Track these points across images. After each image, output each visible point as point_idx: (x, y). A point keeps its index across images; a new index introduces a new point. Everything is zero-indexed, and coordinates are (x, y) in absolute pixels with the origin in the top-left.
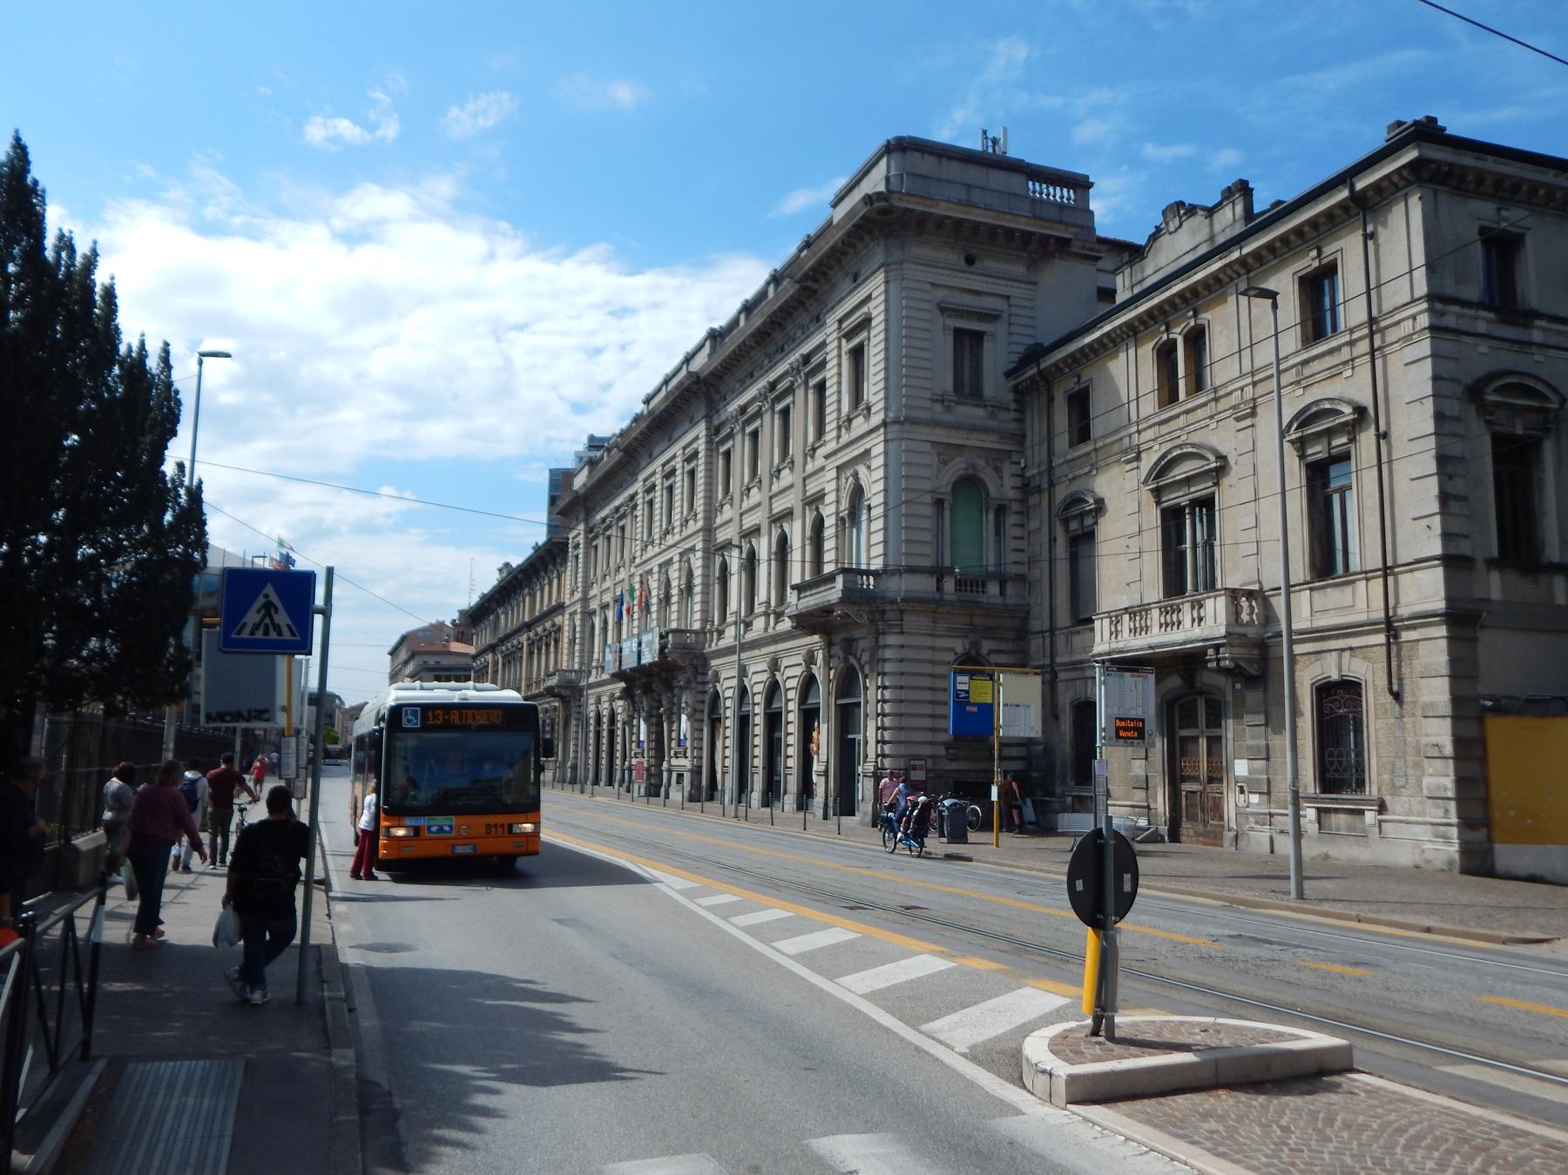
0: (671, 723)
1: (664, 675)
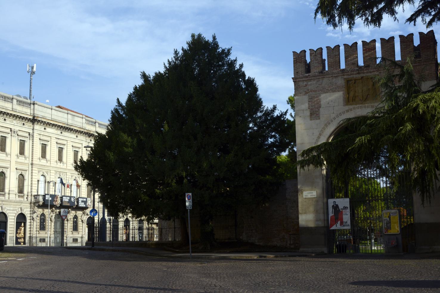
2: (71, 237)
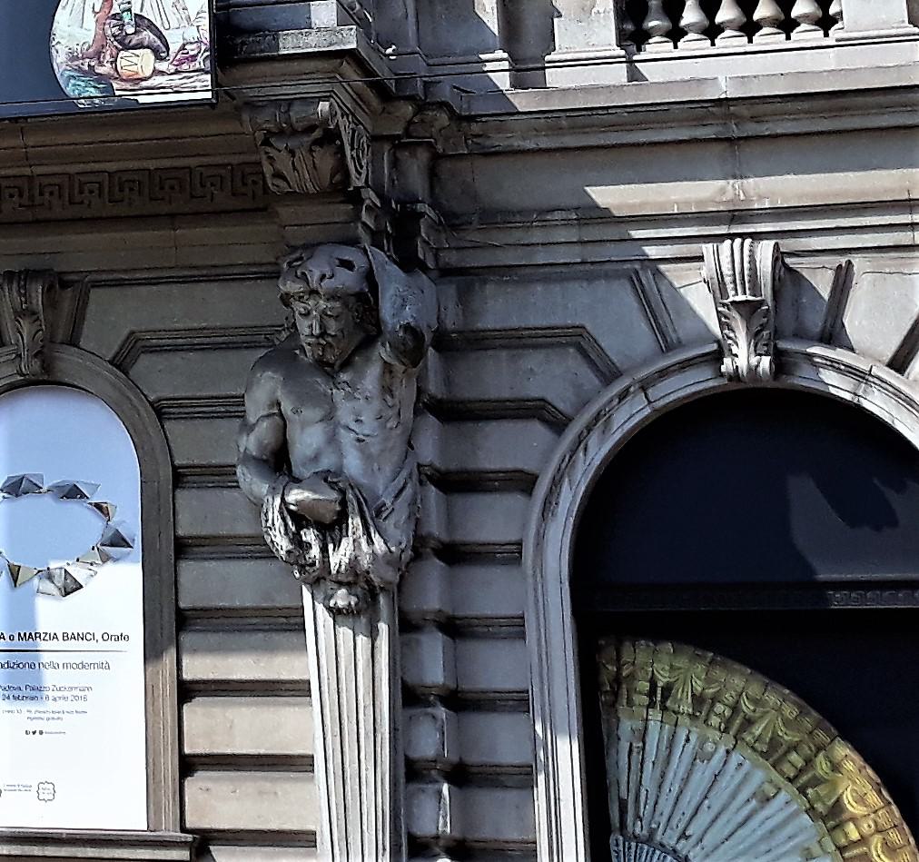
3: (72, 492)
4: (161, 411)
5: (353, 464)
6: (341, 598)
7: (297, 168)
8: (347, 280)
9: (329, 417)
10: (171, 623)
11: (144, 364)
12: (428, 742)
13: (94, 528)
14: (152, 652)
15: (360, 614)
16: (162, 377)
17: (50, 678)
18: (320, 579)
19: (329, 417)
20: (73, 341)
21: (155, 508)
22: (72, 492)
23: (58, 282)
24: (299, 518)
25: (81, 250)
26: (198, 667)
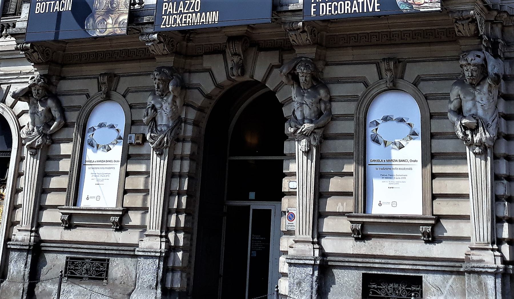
0: (46, 153)
1: (311, 52)
2: (62, 245)
3: (112, 127)
4: (131, 107)
5: (480, 112)
6: (477, 150)
7: (465, 29)
8: (478, 61)
9: (474, 99)
10: (429, 157)
11: (422, 84)
12: (501, 190)
13: (115, 135)
14: (424, 165)
15: (482, 154)
16: (132, 98)
17: (395, 172)
18: (471, 144)
19: (474, 99)
20: (402, 78)
21: (128, 130)
22: (112, 127)
23: (398, 61)
24: (465, 127)
25: (405, 52)
26: (437, 169)
